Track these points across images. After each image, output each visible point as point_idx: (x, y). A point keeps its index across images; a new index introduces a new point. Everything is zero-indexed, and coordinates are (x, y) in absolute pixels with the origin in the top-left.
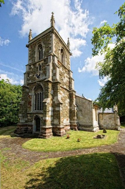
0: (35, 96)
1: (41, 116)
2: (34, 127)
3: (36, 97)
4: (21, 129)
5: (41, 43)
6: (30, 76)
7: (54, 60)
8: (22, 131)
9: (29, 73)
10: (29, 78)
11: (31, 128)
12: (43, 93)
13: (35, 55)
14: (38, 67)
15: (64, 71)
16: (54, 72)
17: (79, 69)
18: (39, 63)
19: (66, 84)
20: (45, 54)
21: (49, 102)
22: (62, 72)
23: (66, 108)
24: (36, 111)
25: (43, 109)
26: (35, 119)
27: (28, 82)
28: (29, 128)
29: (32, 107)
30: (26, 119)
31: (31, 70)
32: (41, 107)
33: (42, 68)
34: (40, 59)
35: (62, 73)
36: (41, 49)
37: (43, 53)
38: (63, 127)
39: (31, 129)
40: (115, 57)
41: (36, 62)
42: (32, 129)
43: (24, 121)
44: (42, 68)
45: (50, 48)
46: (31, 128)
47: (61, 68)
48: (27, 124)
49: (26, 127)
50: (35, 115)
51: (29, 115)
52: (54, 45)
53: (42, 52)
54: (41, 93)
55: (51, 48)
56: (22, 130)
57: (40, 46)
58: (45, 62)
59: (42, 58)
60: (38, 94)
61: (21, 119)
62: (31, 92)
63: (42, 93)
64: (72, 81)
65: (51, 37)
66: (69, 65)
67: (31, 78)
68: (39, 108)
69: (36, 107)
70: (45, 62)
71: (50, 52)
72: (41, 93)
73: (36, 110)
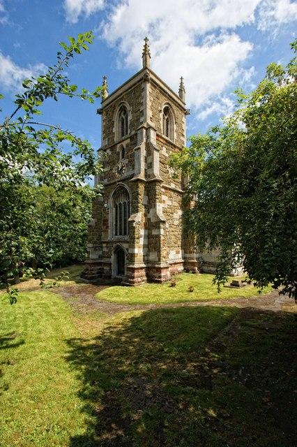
1: (125, 246)
2: (114, 267)
3: (116, 210)
7: (148, 137)
12: (129, 202)
14: (119, 152)
26: (115, 252)
28: (105, 268)
34: (123, 135)
37: (129, 124)
42: (111, 270)
45: (142, 112)
46: (108, 268)
47: (164, 149)
48: (102, 261)
50: (114, 245)
51: (104, 245)
52: (149, 104)
54: (125, 203)
55: (143, 113)
57: (123, 110)
60: (120, 204)
65: (144, 90)
68: (123, 232)
69: (116, 230)
72: (125, 203)
73: (116, 235)
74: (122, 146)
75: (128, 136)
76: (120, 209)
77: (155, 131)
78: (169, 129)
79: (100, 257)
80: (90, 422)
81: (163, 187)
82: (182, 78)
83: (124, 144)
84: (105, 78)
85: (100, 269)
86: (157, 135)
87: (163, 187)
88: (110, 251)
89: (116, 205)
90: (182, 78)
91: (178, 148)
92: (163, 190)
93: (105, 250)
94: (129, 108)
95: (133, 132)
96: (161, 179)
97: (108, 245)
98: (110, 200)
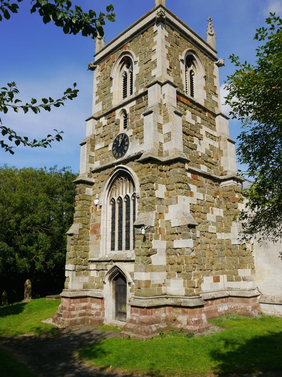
0: (110, 207)
2: (110, 304)
3: (114, 209)
4: (70, 310)
5: (128, 53)
6: (97, 147)
8: (74, 316)
9: (94, 140)
10: (93, 154)
11: (99, 307)
12: (134, 195)
13: (111, 88)
14: (135, 87)
15: (199, 120)
16: (120, 240)
17: (125, 116)
18: (124, 108)
19: (209, 160)
20: (140, 82)
21: (153, 225)
22: (193, 122)
23: (209, 240)
24: (113, 252)
25: (134, 247)
26: (110, 279)
27: (91, 165)
28: (94, 306)
29: (101, 242)
30: (86, 279)
31: (101, 130)
32: (128, 240)
33: (132, 121)
34: (125, 96)
35: (192, 125)
36: (128, 67)
38: (200, 304)
39: (101, 309)
40: (246, 91)
41: (114, 107)
42: (102, 309)
43: (81, 287)
44: (132, 121)
46: (99, 307)
47: (189, 113)
48: (88, 294)
49: (84, 304)
50: (109, 267)
51: (93, 266)
53: (132, 77)
54: (127, 197)
56: (73, 313)
57: (127, 62)
58: (141, 105)
59: (131, 93)
60: (120, 199)
61: (72, 280)
62: (99, 197)
63: (130, 195)
64: (226, 148)
66: (214, 98)
67: (99, 152)
69: (113, 241)
70: (141, 105)
71: (153, 75)
72: (127, 197)
73: (113, 249)
74: (124, 111)
75: (133, 96)
76: (121, 208)
77: (175, 87)
78: (221, 290)
79: (86, 287)
80: (92, 355)
81: (189, 171)
82: (237, 139)
83: (127, 108)
84: (59, 138)
85: (85, 308)
86: (178, 93)
87: (189, 171)
88: (102, 277)
89: (113, 200)
90: (237, 139)
91: (209, 112)
92: (189, 175)
93: (93, 274)
94: (135, 58)
95: (141, 91)
96: (186, 157)
97: (100, 267)
98: (103, 193)
